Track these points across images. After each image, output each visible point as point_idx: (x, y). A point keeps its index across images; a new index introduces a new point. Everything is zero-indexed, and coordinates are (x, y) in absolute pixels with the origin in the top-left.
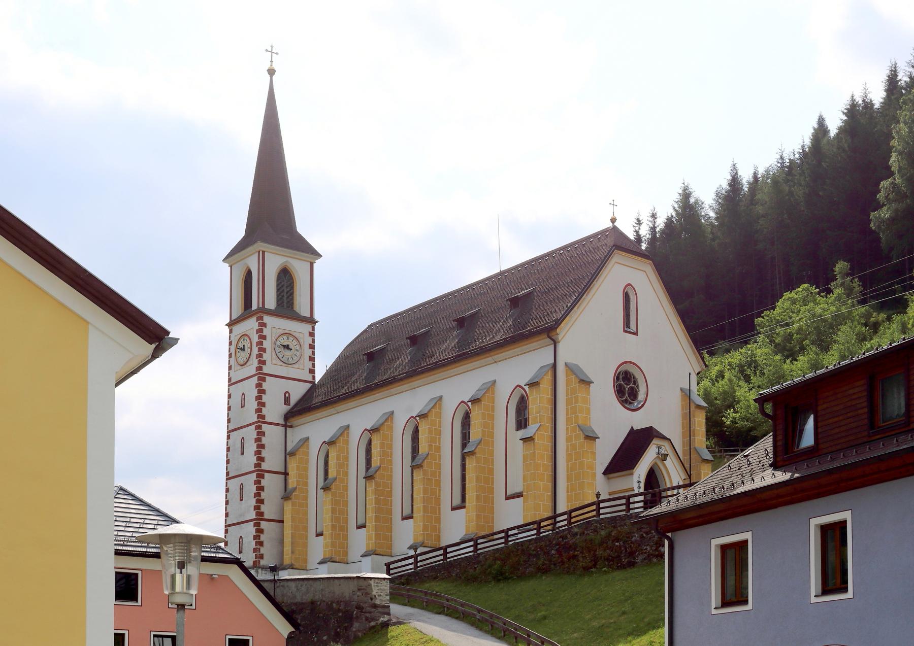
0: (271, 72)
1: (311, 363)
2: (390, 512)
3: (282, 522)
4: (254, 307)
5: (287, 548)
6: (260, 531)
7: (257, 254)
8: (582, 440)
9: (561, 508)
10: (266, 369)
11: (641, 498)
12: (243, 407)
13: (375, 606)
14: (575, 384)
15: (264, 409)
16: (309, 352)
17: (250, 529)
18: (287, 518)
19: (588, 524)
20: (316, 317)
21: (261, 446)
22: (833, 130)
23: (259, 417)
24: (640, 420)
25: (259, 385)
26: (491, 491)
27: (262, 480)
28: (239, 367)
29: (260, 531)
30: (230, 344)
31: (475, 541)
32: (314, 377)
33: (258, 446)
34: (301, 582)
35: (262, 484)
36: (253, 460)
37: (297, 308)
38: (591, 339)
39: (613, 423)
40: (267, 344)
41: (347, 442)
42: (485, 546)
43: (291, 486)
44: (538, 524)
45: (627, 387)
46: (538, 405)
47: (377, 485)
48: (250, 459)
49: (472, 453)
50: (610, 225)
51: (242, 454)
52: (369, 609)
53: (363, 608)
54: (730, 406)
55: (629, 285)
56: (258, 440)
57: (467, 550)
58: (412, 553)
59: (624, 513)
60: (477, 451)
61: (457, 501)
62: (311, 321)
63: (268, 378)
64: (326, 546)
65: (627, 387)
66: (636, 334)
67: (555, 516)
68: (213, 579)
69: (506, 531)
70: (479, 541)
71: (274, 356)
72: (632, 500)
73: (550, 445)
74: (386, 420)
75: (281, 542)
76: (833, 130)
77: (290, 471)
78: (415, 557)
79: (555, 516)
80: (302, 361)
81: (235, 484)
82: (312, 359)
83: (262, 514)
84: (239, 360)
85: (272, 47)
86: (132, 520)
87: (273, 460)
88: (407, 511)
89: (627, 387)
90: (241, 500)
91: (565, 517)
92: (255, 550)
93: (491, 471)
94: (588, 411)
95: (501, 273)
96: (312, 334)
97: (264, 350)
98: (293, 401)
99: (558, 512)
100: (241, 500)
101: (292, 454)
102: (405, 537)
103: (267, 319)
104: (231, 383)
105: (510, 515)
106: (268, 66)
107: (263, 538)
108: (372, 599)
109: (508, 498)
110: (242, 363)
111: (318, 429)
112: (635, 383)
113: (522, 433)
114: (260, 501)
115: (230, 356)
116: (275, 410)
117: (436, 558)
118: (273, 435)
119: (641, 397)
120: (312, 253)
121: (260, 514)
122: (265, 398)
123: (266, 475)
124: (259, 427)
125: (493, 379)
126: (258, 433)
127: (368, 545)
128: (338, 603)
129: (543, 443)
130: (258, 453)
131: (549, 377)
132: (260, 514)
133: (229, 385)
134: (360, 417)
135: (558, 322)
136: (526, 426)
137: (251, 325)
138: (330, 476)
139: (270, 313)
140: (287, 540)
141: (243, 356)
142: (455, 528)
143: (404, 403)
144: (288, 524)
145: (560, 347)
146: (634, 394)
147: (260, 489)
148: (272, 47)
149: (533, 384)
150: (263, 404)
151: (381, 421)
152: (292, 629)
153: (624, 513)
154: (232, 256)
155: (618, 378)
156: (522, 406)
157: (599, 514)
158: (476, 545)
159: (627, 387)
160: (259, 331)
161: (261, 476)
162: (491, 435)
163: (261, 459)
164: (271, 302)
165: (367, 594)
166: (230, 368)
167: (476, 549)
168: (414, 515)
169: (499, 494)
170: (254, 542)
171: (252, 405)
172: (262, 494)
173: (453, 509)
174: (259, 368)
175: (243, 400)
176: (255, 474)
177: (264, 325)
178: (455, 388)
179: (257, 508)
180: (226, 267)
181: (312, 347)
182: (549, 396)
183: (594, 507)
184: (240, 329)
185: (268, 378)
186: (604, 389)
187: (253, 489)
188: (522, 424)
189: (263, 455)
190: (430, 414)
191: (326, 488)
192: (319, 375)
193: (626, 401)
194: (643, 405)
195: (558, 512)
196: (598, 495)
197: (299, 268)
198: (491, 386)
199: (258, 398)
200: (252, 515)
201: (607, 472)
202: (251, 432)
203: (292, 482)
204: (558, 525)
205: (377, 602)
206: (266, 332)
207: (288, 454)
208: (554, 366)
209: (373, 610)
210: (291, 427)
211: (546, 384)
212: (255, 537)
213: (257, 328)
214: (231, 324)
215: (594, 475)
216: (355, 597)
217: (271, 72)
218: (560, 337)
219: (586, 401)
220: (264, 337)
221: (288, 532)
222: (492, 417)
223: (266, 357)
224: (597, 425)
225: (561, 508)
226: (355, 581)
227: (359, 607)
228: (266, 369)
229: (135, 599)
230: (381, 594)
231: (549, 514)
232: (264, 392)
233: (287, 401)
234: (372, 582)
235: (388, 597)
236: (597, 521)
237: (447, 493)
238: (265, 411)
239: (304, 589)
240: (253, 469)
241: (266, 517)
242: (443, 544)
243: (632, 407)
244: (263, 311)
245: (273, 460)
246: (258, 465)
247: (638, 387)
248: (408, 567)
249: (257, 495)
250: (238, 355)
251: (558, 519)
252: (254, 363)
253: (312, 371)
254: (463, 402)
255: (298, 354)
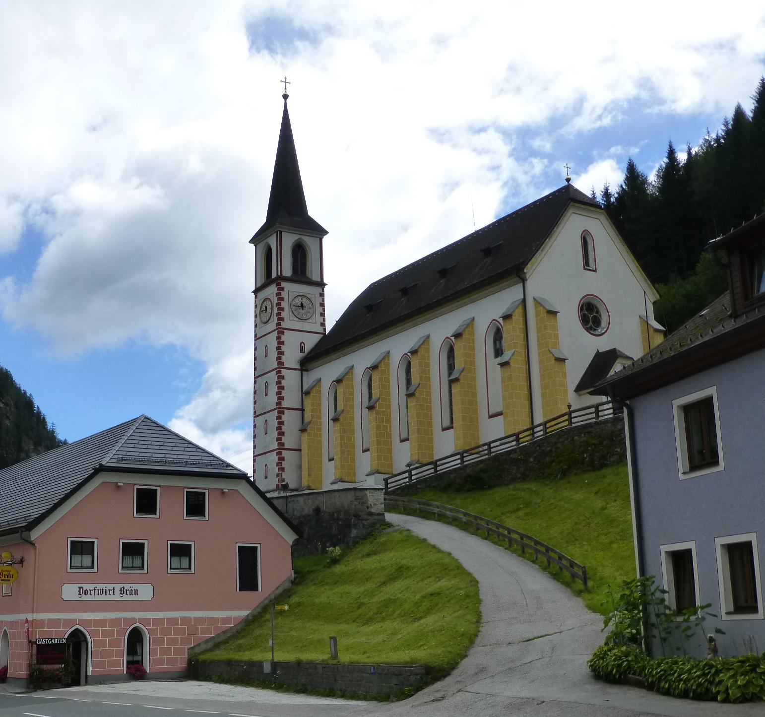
0: (285, 97)
1: (322, 318)
2: (389, 436)
3: (300, 450)
4: (274, 275)
5: (305, 473)
6: (282, 459)
7: (275, 234)
8: (553, 361)
9: (539, 419)
10: (284, 325)
11: (610, 405)
12: (266, 356)
13: (371, 514)
14: (543, 314)
15: (283, 357)
16: (320, 310)
17: (274, 457)
18: (304, 447)
19: (562, 433)
20: (325, 281)
21: (281, 388)
22: (749, 114)
23: (279, 363)
24: (603, 344)
25: (278, 338)
26: (475, 411)
27: (283, 416)
28: (263, 325)
29: (282, 459)
30: (256, 306)
31: (462, 454)
32: (325, 330)
33: (279, 388)
34: (307, 497)
35: (283, 419)
36: (275, 399)
37: (309, 274)
38: (555, 274)
39: (580, 348)
40: (284, 304)
41: (352, 380)
42: (470, 459)
43: (306, 420)
44: (517, 436)
45: (591, 315)
46: (512, 333)
47: (377, 413)
48: (273, 398)
49: (457, 380)
50: (566, 183)
51: (266, 395)
52: (365, 517)
53: (360, 516)
54: (710, 142)
55: (585, 230)
56: (278, 383)
57: (455, 463)
58: (408, 468)
59: (594, 420)
60: (461, 378)
61: (447, 423)
62: (322, 285)
63: (286, 331)
64: (336, 469)
65: (591, 317)
66: (595, 271)
67: (532, 428)
68: (223, 493)
69: (489, 444)
70: (465, 455)
71: (291, 313)
72: (600, 408)
73: (524, 368)
74: (384, 358)
75: (300, 467)
76: (749, 114)
77: (306, 408)
78: (410, 472)
79: (532, 428)
80: (314, 317)
81: (260, 420)
82: (323, 315)
83: (283, 444)
84: (263, 319)
85: (286, 78)
86: (153, 443)
87: (291, 398)
88: (404, 436)
89: (591, 315)
90: (266, 434)
91: (541, 428)
92: (278, 475)
93: (474, 394)
94: (557, 336)
95: (477, 232)
96: (322, 295)
97: (282, 309)
98: (308, 348)
99: (536, 423)
100: (266, 434)
101: (307, 393)
102: (403, 456)
103: (284, 284)
104: (257, 338)
105: (493, 431)
106: (283, 92)
107: (284, 464)
108: (368, 508)
109: (491, 417)
110: (265, 320)
111: (328, 372)
112: (598, 312)
113: (500, 360)
114: (281, 434)
115: (256, 316)
116: (292, 357)
117: (428, 471)
118: (291, 379)
119: (604, 323)
120: (319, 232)
121: (281, 444)
122: (283, 348)
123: (286, 411)
124: (279, 372)
125: (472, 316)
126: (279, 377)
127: (371, 465)
128: (339, 513)
129: (518, 365)
130: (279, 393)
131: (520, 310)
132: (281, 444)
133: (255, 340)
134: (361, 359)
135: (525, 263)
136: (502, 353)
137: (272, 290)
138: (339, 409)
139: (287, 279)
140: (305, 466)
141: (265, 317)
142: (446, 445)
143: (398, 345)
144: (305, 452)
145: (528, 284)
146: (597, 322)
147: (281, 423)
148: (286, 78)
149: (507, 317)
150: (282, 388)
151: (380, 359)
152: (295, 537)
153: (594, 420)
154: (255, 240)
155: (582, 309)
156: (498, 336)
157: (571, 423)
158: (462, 458)
159: (591, 317)
160: (278, 294)
161: (281, 412)
162: (473, 363)
163: (281, 398)
164: (287, 271)
165: (363, 503)
166: (256, 326)
167: (463, 462)
168: (410, 437)
169: (483, 414)
170: (277, 469)
171: (273, 354)
172: (283, 427)
173: (444, 430)
174: (279, 324)
175: (266, 351)
176: (276, 411)
177: (282, 289)
178: (439, 329)
179: (279, 439)
180: (252, 247)
181: (322, 305)
182: (521, 326)
183: (566, 417)
184: (263, 294)
185: (286, 331)
186: (569, 319)
187: (276, 423)
188: (498, 352)
189: (283, 395)
190: (419, 350)
191: (335, 420)
192: (329, 326)
193: (591, 328)
194: (606, 331)
195: (536, 423)
196: (569, 406)
197: (310, 242)
198: (471, 323)
199: (278, 348)
200: (275, 445)
201: (579, 389)
202: (273, 377)
203: (308, 416)
204: (536, 435)
205: (373, 510)
206: (284, 294)
207: (305, 393)
208: (524, 301)
209: (369, 517)
210: (307, 370)
211: (518, 316)
212: (278, 464)
213: (276, 292)
214: (256, 292)
215: (566, 392)
216: (353, 506)
217: (285, 97)
218: (527, 276)
219: (554, 328)
220: (282, 299)
221: (305, 459)
222: (473, 349)
223: (284, 314)
224: (564, 351)
225: (539, 419)
226: (352, 492)
227: (357, 516)
228: (284, 325)
229: (154, 512)
230: (376, 501)
231: (528, 426)
232: (283, 343)
233: (302, 349)
234: (367, 492)
235: (383, 506)
236: (569, 430)
237: (438, 417)
238: (284, 358)
239: (310, 502)
240: (275, 407)
241: (286, 447)
242: (436, 458)
243: (597, 333)
244: (281, 278)
245: (291, 398)
246: (279, 404)
247: (600, 315)
248: (404, 479)
249: (279, 428)
250: (262, 315)
251: (536, 430)
252: (275, 320)
253: (323, 325)
254: (447, 338)
255: (311, 311)
